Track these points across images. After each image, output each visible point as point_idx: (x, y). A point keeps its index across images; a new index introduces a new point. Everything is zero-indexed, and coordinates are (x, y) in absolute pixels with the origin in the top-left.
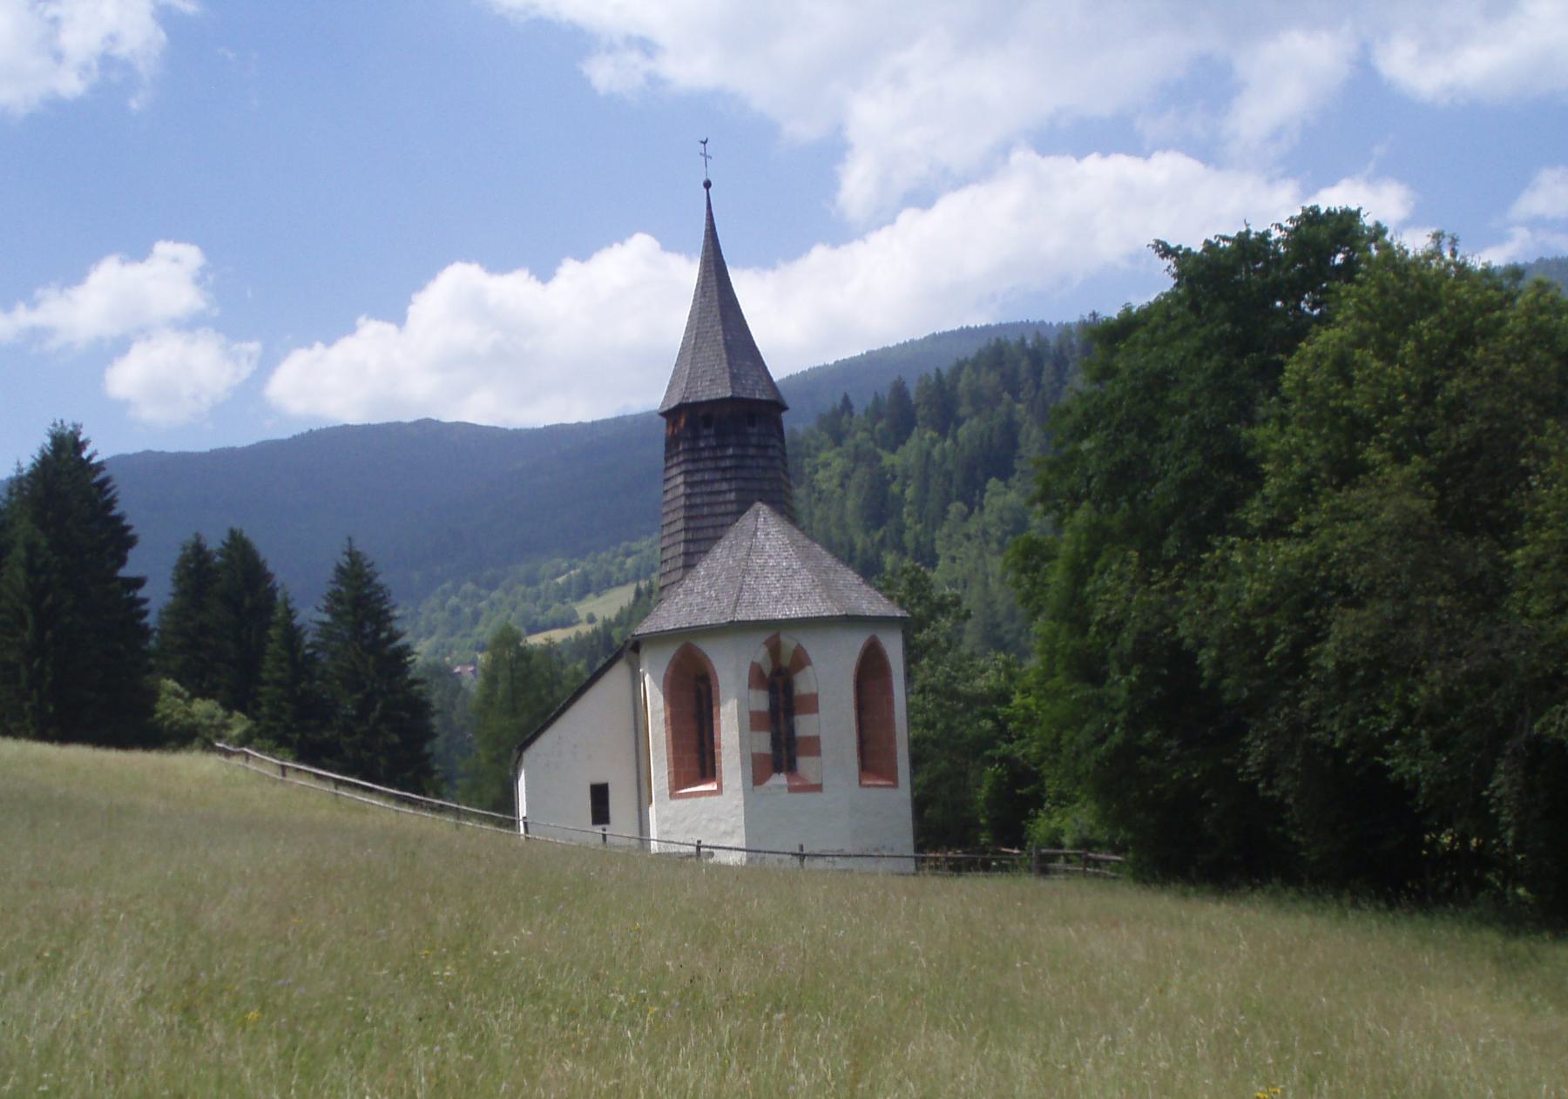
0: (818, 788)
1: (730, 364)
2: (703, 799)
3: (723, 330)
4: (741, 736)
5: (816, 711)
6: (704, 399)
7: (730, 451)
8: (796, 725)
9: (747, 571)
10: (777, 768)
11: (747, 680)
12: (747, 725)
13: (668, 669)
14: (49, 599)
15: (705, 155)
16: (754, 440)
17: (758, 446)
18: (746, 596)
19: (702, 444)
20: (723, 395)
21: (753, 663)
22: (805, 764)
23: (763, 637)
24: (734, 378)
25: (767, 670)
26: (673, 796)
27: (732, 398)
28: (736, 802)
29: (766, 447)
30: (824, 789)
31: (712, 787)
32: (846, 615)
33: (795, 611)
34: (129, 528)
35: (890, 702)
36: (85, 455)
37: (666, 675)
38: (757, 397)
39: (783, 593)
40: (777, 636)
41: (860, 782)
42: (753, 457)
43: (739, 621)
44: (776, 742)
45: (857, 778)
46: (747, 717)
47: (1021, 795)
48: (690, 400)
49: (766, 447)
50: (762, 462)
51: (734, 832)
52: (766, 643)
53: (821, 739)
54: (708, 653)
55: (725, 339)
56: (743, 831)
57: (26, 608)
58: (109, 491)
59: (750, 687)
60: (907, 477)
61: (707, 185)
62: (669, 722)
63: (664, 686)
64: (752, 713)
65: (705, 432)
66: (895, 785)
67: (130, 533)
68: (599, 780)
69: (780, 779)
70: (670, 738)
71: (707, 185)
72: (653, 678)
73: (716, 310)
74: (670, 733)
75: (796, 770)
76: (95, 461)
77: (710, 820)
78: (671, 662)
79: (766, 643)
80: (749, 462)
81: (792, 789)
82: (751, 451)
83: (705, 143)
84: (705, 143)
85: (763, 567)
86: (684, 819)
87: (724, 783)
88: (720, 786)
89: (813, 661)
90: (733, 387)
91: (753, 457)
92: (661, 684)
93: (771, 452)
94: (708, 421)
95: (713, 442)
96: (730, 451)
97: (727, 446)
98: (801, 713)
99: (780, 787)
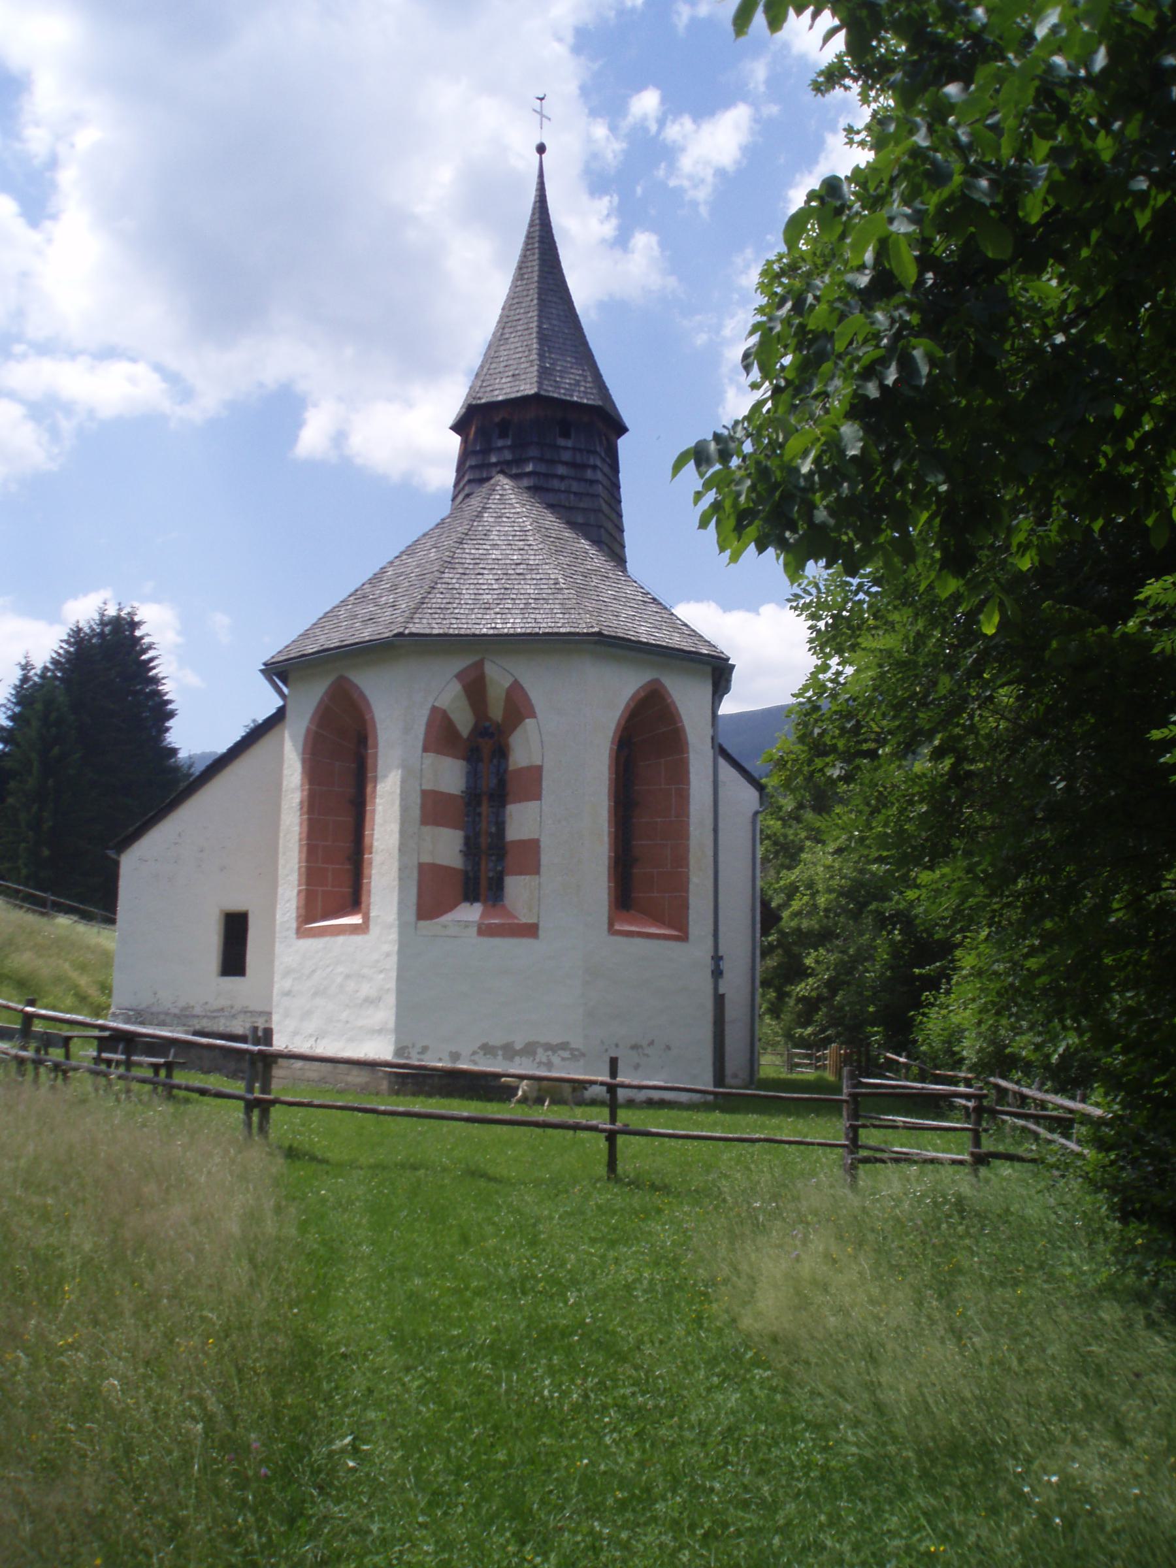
0: (531, 931)
1: (541, 356)
2: (341, 939)
3: (539, 316)
4: (403, 833)
5: (538, 797)
6: (500, 398)
7: (529, 468)
8: (508, 820)
9: (448, 564)
10: (471, 893)
11: (421, 736)
12: (416, 812)
13: (312, 720)
14: (56, 750)
15: (542, 116)
16: (566, 456)
17: (572, 465)
18: (437, 599)
19: (493, 459)
20: (526, 393)
21: (434, 709)
22: (516, 887)
23: (459, 664)
24: (544, 373)
25: (464, 722)
26: (301, 933)
27: (536, 396)
28: (386, 948)
29: (584, 466)
30: (541, 933)
31: (356, 920)
32: (599, 634)
33: (514, 624)
34: (169, 702)
35: (683, 797)
36: (138, 633)
37: (308, 730)
38: (575, 399)
39: (501, 599)
40: (479, 665)
41: (611, 924)
42: (562, 478)
43: (412, 635)
44: (471, 849)
45: (605, 919)
46: (416, 800)
47: (921, 975)
48: (483, 401)
49: (584, 466)
50: (575, 486)
51: (380, 999)
52: (459, 676)
53: (542, 844)
54: (367, 693)
55: (539, 327)
56: (391, 999)
57: (34, 755)
58: (154, 668)
59: (425, 749)
60: (1048, 1032)
61: (541, 149)
62: (305, 809)
63: (304, 752)
64: (425, 794)
65: (500, 443)
66: (683, 936)
67: (170, 707)
68: (236, 906)
69: (471, 913)
70: (304, 835)
71: (541, 149)
72: (292, 737)
73: (534, 294)
74: (305, 829)
75: (502, 900)
76: (146, 640)
77: (348, 977)
78: (318, 707)
79: (459, 676)
80: (556, 484)
81: (485, 931)
82: (561, 470)
83: (541, 99)
84: (541, 99)
85: (477, 561)
86: (314, 971)
87: (373, 914)
88: (366, 918)
89: (537, 710)
90: (540, 383)
91: (562, 478)
92: (300, 747)
93: (589, 474)
94: (503, 429)
95: (508, 455)
96: (529, 468)
97: (528, 460)
98: (514, 802)
99: (467, 925)
